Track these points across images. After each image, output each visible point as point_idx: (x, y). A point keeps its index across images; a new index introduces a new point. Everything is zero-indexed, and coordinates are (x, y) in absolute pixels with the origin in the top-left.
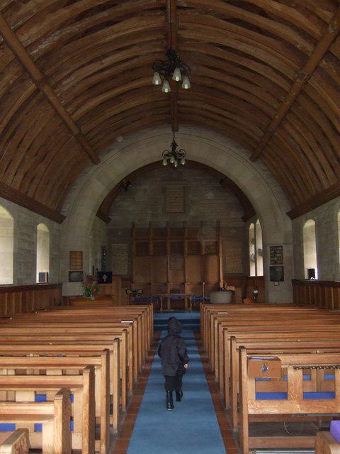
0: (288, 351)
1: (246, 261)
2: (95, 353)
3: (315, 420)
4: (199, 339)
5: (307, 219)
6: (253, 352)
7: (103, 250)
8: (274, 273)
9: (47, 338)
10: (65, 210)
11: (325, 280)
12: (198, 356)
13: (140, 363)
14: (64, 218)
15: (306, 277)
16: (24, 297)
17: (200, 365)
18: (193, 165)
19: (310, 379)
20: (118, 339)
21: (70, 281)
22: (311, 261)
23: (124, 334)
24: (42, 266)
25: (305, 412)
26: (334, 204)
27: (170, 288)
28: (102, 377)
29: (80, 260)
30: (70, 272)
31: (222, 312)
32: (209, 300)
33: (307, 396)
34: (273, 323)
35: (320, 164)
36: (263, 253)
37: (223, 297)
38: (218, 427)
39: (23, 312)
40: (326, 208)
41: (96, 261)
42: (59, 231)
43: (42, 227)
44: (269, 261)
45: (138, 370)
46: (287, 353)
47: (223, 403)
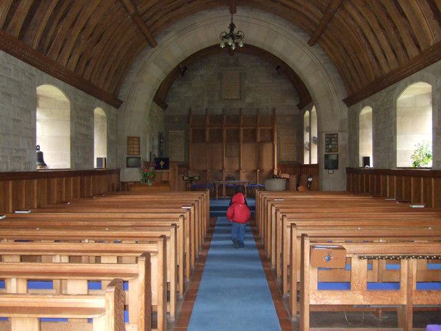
0: (350, 239)
1: (300, 149)
2: (152, 240)
3: (375, 310)
4: (254, 226)
5: (364, 106)
6: (315, 239)
7: (160, 136)
8: (329, 162)
9: (104, 223)
10: (122, 95)
11: (380, 168)
12: (253, 242)
13: (197, 249)
14: (122, 102)
15: (361, 165)
16: (82, 183)
17: (256, 252)
18: (251, 50)
19: (372, 269)
20: (175, 225)
21: (128, 166)
22: (367, 149)
23: (181, 220)
24: (100, 151)
25: (369, 304)
26: (393, 90)
27: (225, 175)
28: (159, 264)
29: (137, 150)
30: (128, 158)
31: (279, 199)
32: (264, 187)
33: (371, 286)
34: (331, 210)
35: (380, 46)
36: (318, 141)
37: (278, 184)
38: (275, 316)
39: (81, 197)
40: (385, 94)
41: (153, 147)
42: (116, 115)
43: (99, 111)
44: (324, 150)
45: (195, 256)
46: (367, 242)
47: (280, 290)
